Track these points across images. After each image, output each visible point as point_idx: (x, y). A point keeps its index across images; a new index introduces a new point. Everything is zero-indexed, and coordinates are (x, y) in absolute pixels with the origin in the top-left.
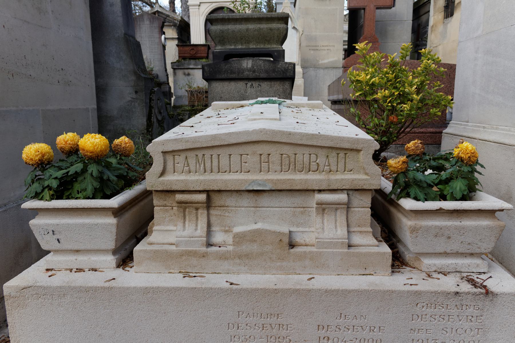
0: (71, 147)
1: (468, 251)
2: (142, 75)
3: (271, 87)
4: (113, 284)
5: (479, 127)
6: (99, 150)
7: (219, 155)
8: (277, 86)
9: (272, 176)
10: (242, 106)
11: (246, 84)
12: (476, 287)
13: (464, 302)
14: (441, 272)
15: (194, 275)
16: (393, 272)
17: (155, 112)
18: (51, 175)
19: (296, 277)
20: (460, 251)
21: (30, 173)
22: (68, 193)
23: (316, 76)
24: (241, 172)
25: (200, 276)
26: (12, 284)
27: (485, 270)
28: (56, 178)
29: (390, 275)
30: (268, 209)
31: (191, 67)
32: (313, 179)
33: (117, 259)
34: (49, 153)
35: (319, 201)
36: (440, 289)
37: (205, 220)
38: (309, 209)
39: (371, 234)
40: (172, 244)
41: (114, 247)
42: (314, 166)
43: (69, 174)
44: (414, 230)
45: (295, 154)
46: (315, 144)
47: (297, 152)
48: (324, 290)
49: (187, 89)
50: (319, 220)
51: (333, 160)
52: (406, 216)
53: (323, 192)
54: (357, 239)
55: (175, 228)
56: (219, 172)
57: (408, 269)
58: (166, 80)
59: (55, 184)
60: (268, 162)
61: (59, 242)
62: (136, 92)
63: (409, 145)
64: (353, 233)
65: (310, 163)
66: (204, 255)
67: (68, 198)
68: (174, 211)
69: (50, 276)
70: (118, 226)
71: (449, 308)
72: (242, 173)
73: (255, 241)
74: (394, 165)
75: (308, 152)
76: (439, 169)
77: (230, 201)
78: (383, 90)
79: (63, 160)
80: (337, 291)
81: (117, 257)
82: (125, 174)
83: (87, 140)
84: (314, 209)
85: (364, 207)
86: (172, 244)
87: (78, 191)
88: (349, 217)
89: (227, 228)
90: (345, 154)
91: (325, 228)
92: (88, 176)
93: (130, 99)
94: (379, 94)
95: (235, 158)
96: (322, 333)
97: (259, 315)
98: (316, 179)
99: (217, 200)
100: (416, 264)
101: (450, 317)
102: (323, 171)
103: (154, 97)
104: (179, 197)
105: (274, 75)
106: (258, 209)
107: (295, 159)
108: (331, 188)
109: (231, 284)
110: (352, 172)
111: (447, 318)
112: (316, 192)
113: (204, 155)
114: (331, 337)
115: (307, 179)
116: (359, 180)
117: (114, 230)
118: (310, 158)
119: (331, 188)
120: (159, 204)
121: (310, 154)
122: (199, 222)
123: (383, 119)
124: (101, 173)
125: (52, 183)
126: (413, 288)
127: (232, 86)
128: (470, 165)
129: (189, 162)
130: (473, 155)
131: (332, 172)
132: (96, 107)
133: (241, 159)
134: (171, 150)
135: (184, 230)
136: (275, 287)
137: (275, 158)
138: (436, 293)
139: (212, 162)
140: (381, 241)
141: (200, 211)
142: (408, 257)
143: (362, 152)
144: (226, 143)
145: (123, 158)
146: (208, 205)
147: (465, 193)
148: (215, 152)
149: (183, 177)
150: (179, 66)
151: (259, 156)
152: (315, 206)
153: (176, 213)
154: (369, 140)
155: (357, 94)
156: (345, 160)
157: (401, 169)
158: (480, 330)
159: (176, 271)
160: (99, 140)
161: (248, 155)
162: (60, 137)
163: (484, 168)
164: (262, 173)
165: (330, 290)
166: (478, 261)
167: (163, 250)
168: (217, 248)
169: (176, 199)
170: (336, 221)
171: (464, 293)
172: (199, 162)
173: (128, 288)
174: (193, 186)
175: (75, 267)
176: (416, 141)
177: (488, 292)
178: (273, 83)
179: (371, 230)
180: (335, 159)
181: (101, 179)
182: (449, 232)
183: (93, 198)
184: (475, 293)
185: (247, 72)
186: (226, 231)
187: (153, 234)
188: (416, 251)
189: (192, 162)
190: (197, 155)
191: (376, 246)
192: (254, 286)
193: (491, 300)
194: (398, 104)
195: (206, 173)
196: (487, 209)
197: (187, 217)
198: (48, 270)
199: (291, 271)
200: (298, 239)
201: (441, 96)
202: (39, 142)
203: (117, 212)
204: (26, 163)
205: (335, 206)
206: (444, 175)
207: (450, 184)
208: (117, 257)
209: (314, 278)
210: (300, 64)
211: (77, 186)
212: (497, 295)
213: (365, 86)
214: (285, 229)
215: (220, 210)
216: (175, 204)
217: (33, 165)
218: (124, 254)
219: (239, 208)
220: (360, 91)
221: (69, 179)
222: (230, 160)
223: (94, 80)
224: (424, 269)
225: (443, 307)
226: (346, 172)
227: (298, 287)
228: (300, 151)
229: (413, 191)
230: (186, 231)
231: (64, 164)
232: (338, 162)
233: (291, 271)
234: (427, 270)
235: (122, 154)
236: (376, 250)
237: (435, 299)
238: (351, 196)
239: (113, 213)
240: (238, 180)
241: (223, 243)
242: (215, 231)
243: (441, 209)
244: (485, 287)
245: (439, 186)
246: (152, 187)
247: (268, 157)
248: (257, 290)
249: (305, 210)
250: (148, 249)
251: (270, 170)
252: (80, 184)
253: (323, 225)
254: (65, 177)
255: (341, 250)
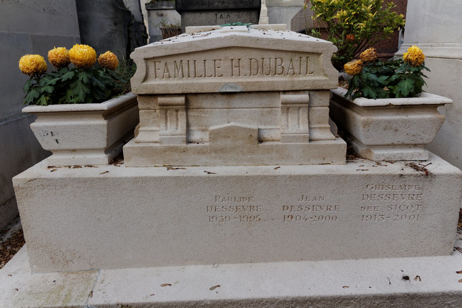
0: (62, 60)
1: (412, 142)
2: (120, 7)
3: (239, 17)
4: (107, 175)
5: (427, 46)
6: (87, 58)
7: (195, 61)
8: (244, 15)
9: (241, 79)
10: (214, 30)
11: (216, 15)
12: (417, 170)
13: (407, 183)
14: (388, 161)
15: (176, 167)
16: (347, 162)
17: (133, 43)
18: (46, 83)
19: (264, 167)
20: (405, 143)
21: (27, 82)
22: (63, 99)
23: (280, 15)
24: (215, 76)
25: (181, 168)
26: (20, 177)
27: (426, 158)
28: (51, 85)
29: (345, 163)
30: (239, 110)
31: (164, 7)
32: (279, 81)
33: (109, 157)
34: (43, 63)
35: (284, 101)
36: (387, 173)
37: (184, 121)
38: (275, 109)
39: (329, 130)
40: (156, 142)
41: (106, 146)
42: (279, 70)
43: (62, 81)
44: (366, 124)
45: (263, 59)
46: (280, 48)
47: (265, 57)
48: (289, 176)
49: (161, 27)
50: (284, 118)
51: (296, 64)
52: (359, 114)
53: (287, 93)
54: (317, 134)
55: (158, 129)
56: (195, 77)
57: (360, 160)
58: (141, 20)
59: (50, 90)
60: (239, 66)
61: (58, 142)
62: (115, 24)
63: (363, 53)
64: (314, 130)
65: (276, 66)
66: (185, 151)
67: (62, 103)
68: (157, 113)
69: (52, 171)
70: (108, 125)
71: (394, 188)
72: (216, 77)
73: (228, 137)
74: (351, 68)
75: (274, 57)
76: (390, 74)
77: (205, 103)
78: (341, 11)
79: (55, 72)
80: (300, 176)
81: (109, 155)
82: (112, 85)
83: (76, 49)
84: (280, 109)
85: (323, 106)
86: (156, 142)
87: (71, 97)
88: (310, 116)
89: (204, 128)
90: (307, 57)
91: (289, 125)
92: (79, 82)
93: (110, 31)
94: (338, 14)
95: (210, 64)
96: (287, 212)
97: (233, 199)
98: (281, 81)
99: (195, 102)
100: (367, 156)
101: (395, 196)
102: (287, 74)
103: (132, 29)
104: (161, 100)
105: (241, 6)
106: (230, 110)
107: (263, 64)
108: (294, 89)
109: (209, 173)
110: (313, 74)
111: (392, 197)
112: (281, 93)
113: (181, 61)
114: (294, 216)
115: (273, 81)
116: (319, 81)
117: (105, 130)
118: (276, 62)
119: (294, 89)
120: (143, 107)
121: (276, 59)
122: (179, 122)
123: (341, 38)
124: (91, 80)
125: (47, 89)
126: (365, 172)
127: (204, 16)
128: (418, 67)
129: (169, 68)
130: (420, 57)
131: (295, 75)
132: (79, 36)
133: (215, 64)
134: (152, 56)
135: (166, 129)
136: (246, 175)
137: (245, 62)
138: (384, 175)
139: (189, 67)
140: (338, 137)
141: (180, 113)
142: (361, 150)
143: (322, 55)
144: (201, 49)
145: (109, 70)
146: (187, 107)
147: (412, 91)
148: (191, 58)
149: (163, 82)
150: (153, 7)
151: (230, 61)
152: (280, 105)
153: (159, 115)
154: (329, 44)
155: (318, 16)
156: (307, 63)
157: (356, 71)
158: (420, 206)
159: (160, 165)
160: (87, 49)
161: (220, 60)
162: (51, 51)
163: (430, 71)
164: (233, 76)
165: (294, 176)
166: (421, 151)
167: (149, 147)
168: (196, 145)
169: (159, 102)
170: (299, 118)
171: (407, 175)
172: (177, 68)
173: (120, 178)
174: (173, 89)
175: (73, 164)
176: (370, 49)
177: (427, 174)
178: (240, 14)
179: (329, 126)
180: (298, 62)
181: (90, 85)
182: (396, 126)
183: (85, 102)
184: (417, 175)
185: (217, 3)
186: (203, 130)
187: (140, 134)
188: (368, 143)
189: (171, 67)
190: (175, 61)
191: (333, 140)
192: (229, 174)
193: (430, 181)
194: (354, 23)
195: (184, 78)
196: (430, 103)
197: (169, 119)
198: (49, 167)
199: (260, 163)
200: (266, 135)
201: (394, 15)
202: (34, 54)
203: (108, 114)
204: (23, 72)
205: (298, 105)
206: (394, 77)
207: (399, 84)
208: (109, 155)
209: (279, 167)
210: (265, 3)
211: (70, 93)
212: (435, 176)
213: (325, 7)
214: (255, 126)
215: (197, 111)
216: (157, 107)
217: (29, 74)
218: (114, 153)
219: (214, 110)
220: (321, 12)
221: (62, 86)
222: (205, 66)
223: (76, 11)
224: (374, 159)
225: (389, 188)
226: (307, 74)
227: (266, 174)
228: (267, 55)
229: (366, 92)
230: (168, 130)
231: (56, 75)
232: (300, 65)
233: (260, 163)
234: (376, 160)
235: (108, 67)
236: (333, 142)
237: (382, 181)
238: (312, 96)
239: (103, 116)
240: (213, 83)
241: (201, 140)
242: (193, 130)
243: (390, 105)
244: (425, 170)
245: (389, 87)
246: (137, 91)
247: (239, 62)
248: (230, 177)
249: (272, 110)
250: (135, 146)
251: (241, 74)
252: (72, 90)
253: (288, 122)
254: (58, 85)
255: (303, 143)
